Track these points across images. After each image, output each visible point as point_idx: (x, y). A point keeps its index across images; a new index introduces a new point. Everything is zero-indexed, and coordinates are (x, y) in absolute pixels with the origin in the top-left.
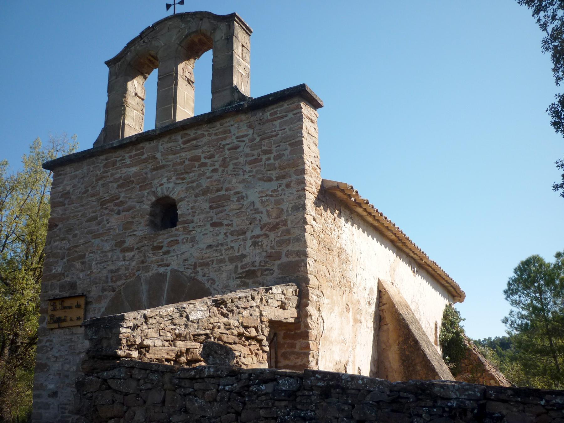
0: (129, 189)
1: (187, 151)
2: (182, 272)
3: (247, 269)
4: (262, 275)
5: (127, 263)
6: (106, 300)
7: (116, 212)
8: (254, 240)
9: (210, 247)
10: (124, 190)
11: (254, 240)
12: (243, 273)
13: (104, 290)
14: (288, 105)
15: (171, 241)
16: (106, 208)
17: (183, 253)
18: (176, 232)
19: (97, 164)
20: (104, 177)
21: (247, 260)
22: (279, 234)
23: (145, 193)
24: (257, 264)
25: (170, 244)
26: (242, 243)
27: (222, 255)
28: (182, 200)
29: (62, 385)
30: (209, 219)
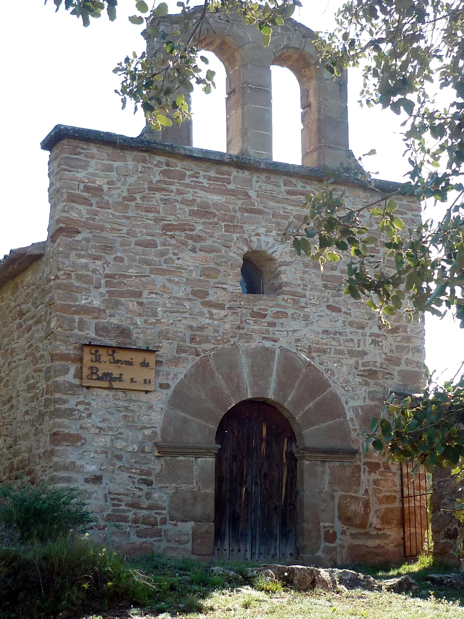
0: (210, 223)
1: (292, 205)
2: (295, 353)
3: (369, 368)
4: (383, 377)
5: (216, 323)
6: (185, 364)
7: (189, 248)
8: (373, 338)
9: (326, 332)
10: (202, 221)
11: (373, 338)
12: (364, 371)
13: (180, 350)
14: (407, 201)
15: (280, 312)
16: (172, 237)
17: (294, 331)
18: (284, 303)
19: (149, 165)
20: (165, 190)
21: (367, 358)
22: (399, 339)
23: (235, 236)
24: (378, 364)
25: (278, 315)
26: (362, 338)
27: (340, 345)
28: (286, 264)
29: (111, 468)
30: (325, 300)
